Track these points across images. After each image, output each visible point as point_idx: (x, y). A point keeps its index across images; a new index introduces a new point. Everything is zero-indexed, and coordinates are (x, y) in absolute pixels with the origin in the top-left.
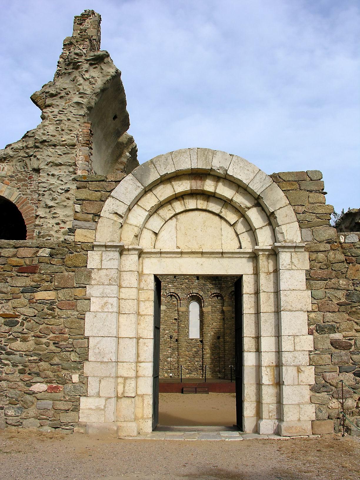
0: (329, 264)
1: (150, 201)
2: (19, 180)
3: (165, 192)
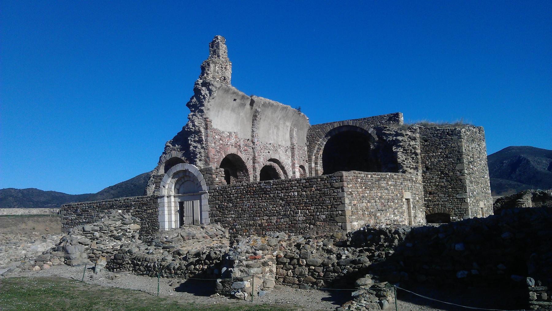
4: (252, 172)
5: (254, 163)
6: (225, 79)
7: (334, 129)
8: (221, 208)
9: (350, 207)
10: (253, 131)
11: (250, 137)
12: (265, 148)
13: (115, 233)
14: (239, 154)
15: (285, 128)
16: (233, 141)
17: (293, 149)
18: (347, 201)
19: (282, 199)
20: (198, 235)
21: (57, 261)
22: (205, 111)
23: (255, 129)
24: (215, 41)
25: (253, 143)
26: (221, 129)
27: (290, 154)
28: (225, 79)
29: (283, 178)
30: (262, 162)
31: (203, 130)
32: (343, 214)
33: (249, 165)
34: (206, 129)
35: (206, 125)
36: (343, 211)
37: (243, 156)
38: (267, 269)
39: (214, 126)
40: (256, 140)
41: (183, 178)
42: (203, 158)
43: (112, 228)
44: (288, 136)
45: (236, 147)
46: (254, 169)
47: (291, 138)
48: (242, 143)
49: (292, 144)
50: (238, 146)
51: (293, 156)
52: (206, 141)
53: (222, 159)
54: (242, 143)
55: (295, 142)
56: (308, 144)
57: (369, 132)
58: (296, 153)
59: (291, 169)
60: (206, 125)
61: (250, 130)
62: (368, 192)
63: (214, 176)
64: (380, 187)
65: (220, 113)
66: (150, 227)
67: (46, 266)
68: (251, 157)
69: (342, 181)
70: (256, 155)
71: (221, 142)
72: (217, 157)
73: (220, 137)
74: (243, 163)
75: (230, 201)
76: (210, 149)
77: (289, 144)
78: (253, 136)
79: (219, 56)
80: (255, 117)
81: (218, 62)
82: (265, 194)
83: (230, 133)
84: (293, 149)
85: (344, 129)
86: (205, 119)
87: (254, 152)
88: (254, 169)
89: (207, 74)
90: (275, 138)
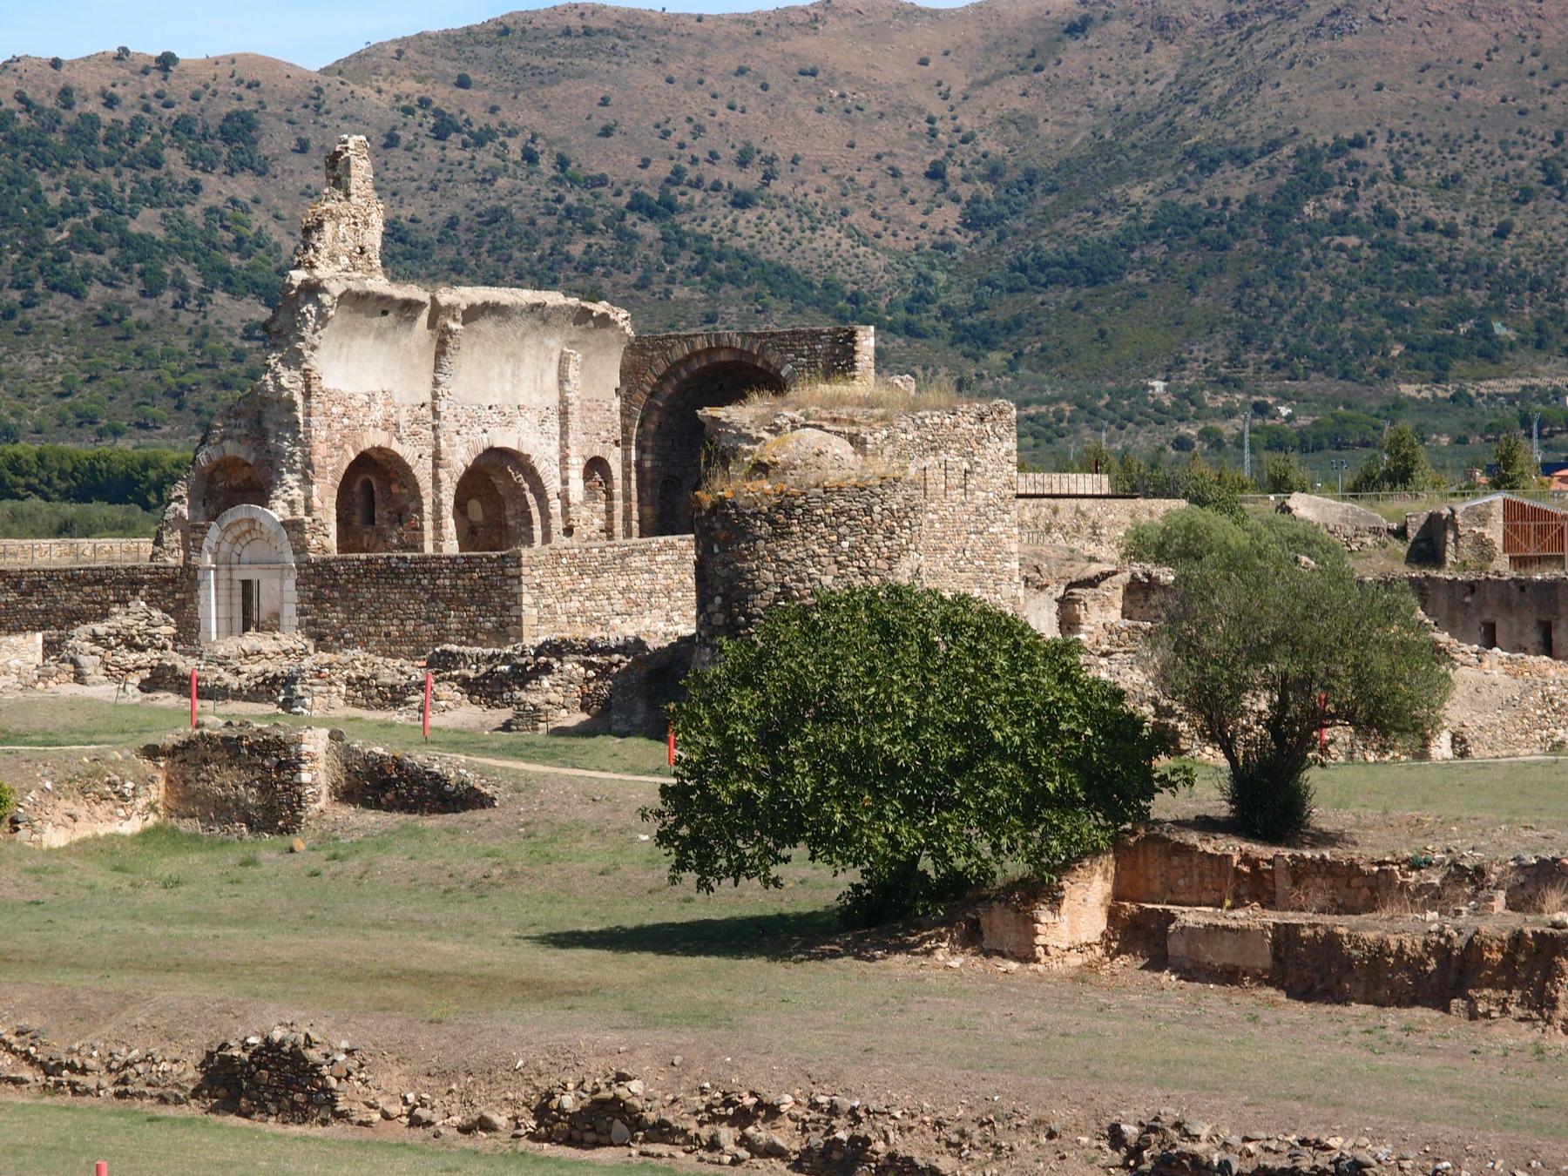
0: (307, 576)
1: (229, 537)
2: (254, 439)
3: (236, 531)
4: (430, 490)
5: (436, 466)
6: (362, 252)
7: (695, 354)
8: (318, 600)
9: (535, 611)
10: (436, 383)
11: (427, 398)
12: (474, 419)
13: (138, 639)
14: (396, 447)
15: (542, 356)
16: (377, 414)
17: (564, 414)
18: (527, 599)
19: (424, 589)
20: (266, 649)
21: (63, 676)
22: (306, 353)
23: (441, 378)
24: (340, 153)
25: (436, 414)
26: (347, 389)
27: (557, 428)
28: (362, 252)
29: (429, 549)
30: (460, 457)
31: (298, 398)
32: (519, 622)
33: (422, 473)
34: (307, 395)
35: (308, 386)
36: (519, 617)
37: (407, 451)
38: (334, 689)
39: (327, 383)
40: (442, 406)
41: (249, 532)
42: (299, 466)
43: (134, 632)
44: (552, 376)
45: (385, 429)
46: (436, 482)
47: (563, 380)
48: (404, 418)
49: (564, 401)
50: (391, 426)
51: (564, 434)
52: (307, 424)
53: (346, 465)
54: (404, 418)
55: (571, 395)
56: (624, 391)
57: (783, 373)
58: (574, 423)
59: (557, 470)
60: (308, 386)
61: (429, 379)
62: (588, 581)
63: (308, 536)
64: (624, 568)
65: (345, 350)
66: (188, 634)
67: (51, 684)
68: (430, 451)
69: (520, 565)
70: (443, 443)
71: (346, 421)
72: (334, 460)
73: (341, 410)
74: (407, 469)
75: (335, 586)
76: (315, 443)
77: (553, 399)
78: (435, 396)
79: (348, 195)
80: (441, 351)
81: (344, 212)
82: (397, 577)
83: (371, 395)
84: (564, 414)
85: (723, 357)
86: (306, 373)
87: (437, 438)
88: (436, 482)
89: (316, 251)
90: (508, 387)
